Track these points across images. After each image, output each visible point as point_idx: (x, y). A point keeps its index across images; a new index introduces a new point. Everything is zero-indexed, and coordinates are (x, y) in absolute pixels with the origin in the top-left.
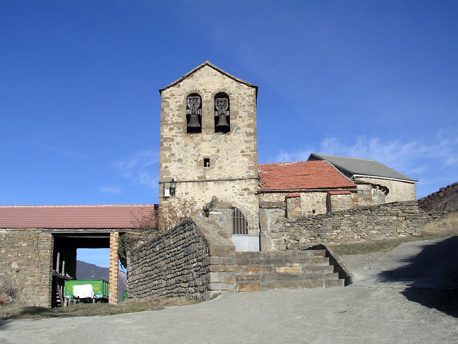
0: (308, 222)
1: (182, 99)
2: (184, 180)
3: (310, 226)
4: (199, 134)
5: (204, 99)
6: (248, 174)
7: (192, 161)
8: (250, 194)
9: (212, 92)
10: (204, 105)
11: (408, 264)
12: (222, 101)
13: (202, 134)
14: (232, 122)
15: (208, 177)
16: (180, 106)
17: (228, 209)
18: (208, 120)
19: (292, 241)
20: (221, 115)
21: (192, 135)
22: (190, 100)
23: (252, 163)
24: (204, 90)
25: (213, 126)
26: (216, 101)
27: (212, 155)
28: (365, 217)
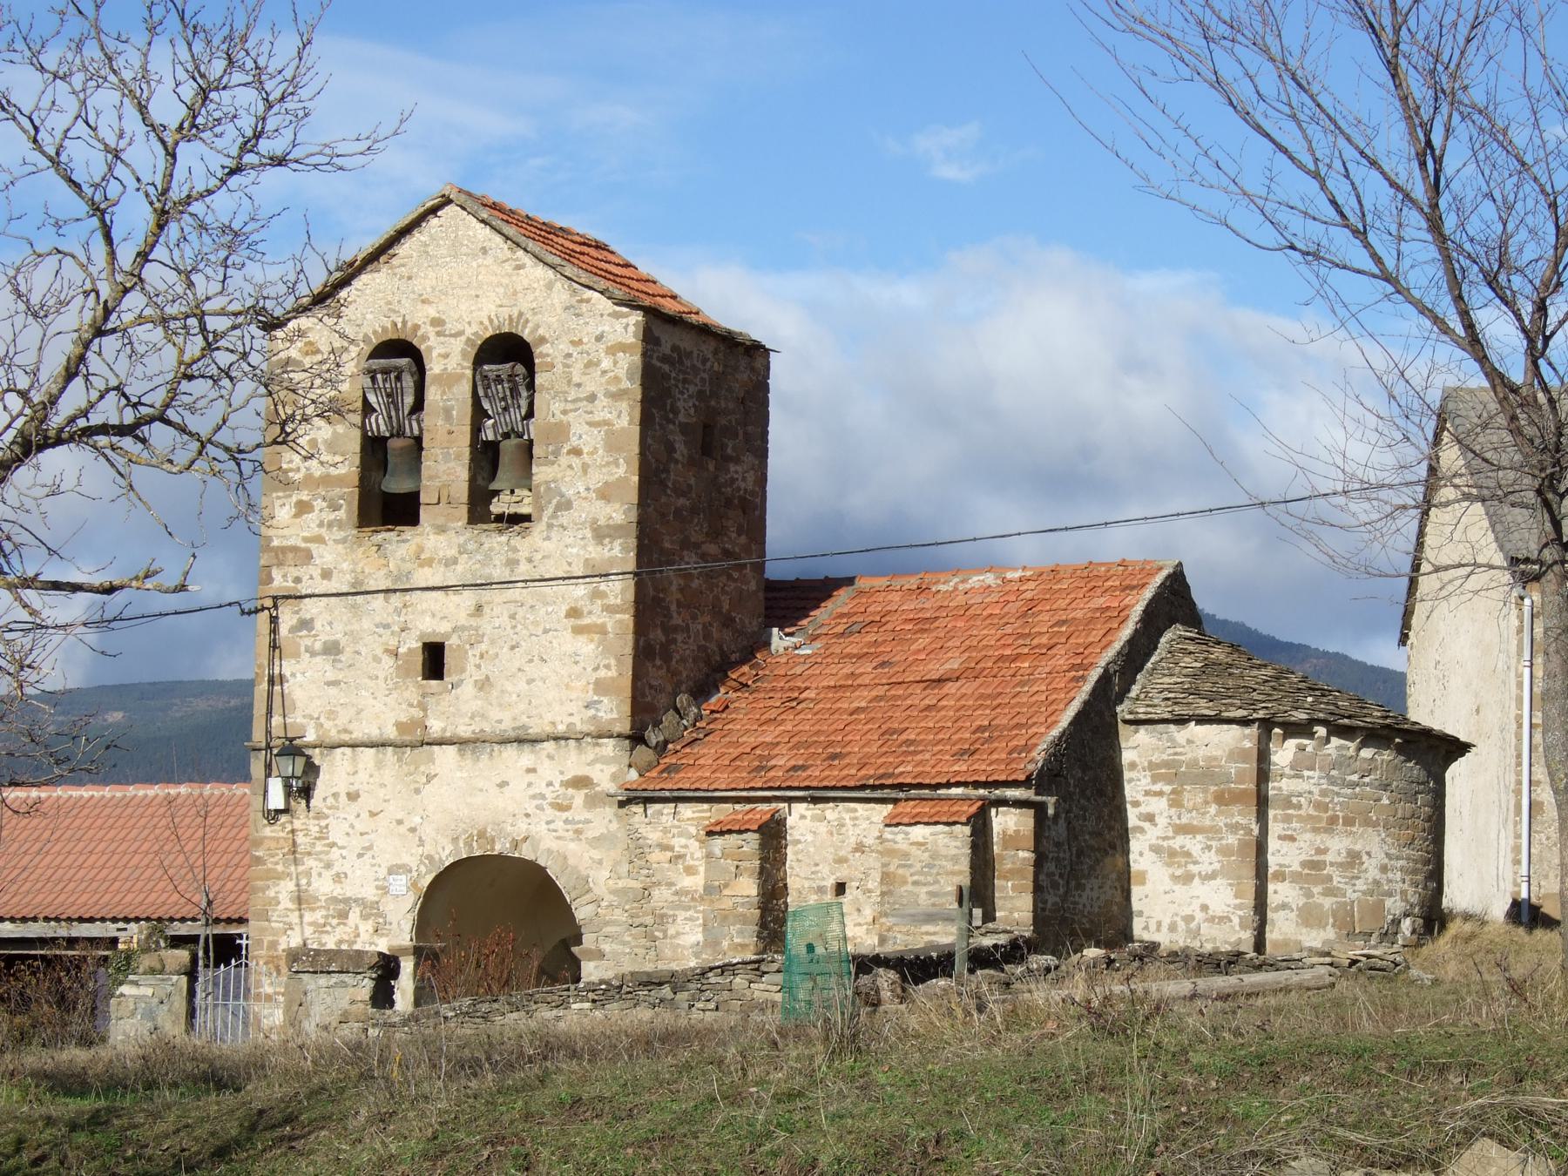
2: (346, 737)
6: (592, 712)
13: (419, 529)
15: (436, 727)
18: (445, 468)
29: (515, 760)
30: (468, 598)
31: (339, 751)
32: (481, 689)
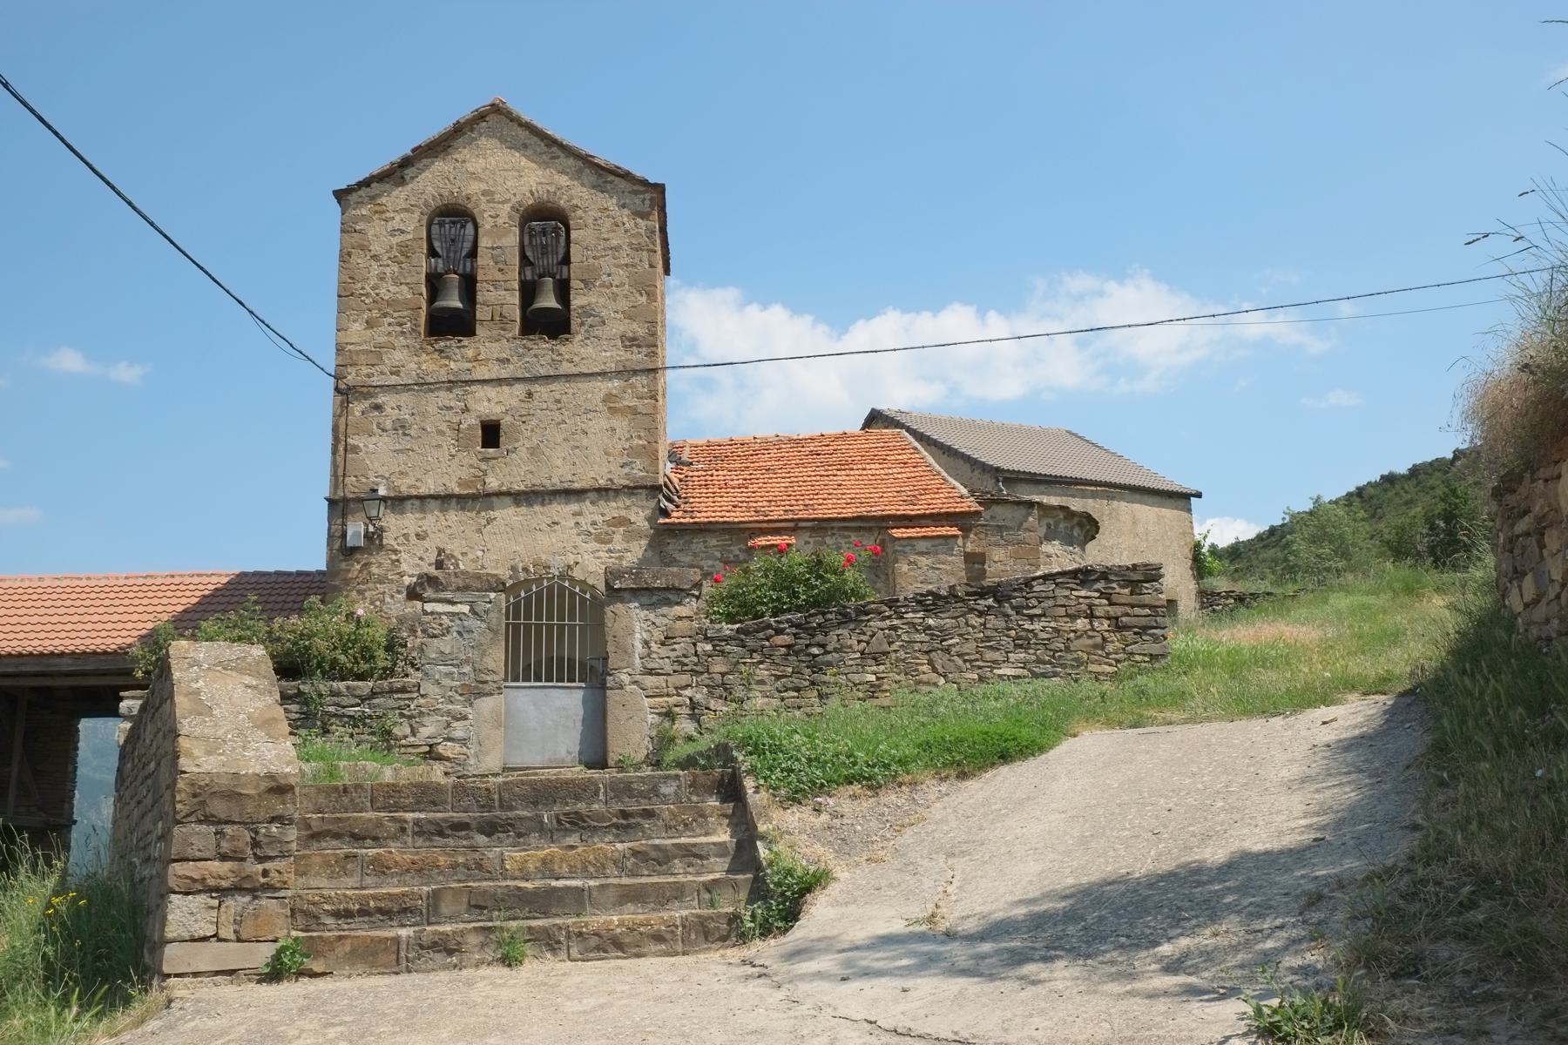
0: (780, 640)
1: (412, 226)
3: (783, 650)
4: (466, 341)
5: (486, 224)
6: (627, 470)
7: (444, 427)
8: (630, 536)
9: (514, 200)
10: (484, 242)
11: (1061, 905)
12: (544, 232)
14: (577, 301)
15: (493, 483)
16: (405, 250)
17: (492, 595)
18: (500, 295)
20: (541, 276)
22: (441, 225)
23: (640, 437)
24: (484, 193)
28: (975, 620)
29: (562, 510)
30: (519, 390)
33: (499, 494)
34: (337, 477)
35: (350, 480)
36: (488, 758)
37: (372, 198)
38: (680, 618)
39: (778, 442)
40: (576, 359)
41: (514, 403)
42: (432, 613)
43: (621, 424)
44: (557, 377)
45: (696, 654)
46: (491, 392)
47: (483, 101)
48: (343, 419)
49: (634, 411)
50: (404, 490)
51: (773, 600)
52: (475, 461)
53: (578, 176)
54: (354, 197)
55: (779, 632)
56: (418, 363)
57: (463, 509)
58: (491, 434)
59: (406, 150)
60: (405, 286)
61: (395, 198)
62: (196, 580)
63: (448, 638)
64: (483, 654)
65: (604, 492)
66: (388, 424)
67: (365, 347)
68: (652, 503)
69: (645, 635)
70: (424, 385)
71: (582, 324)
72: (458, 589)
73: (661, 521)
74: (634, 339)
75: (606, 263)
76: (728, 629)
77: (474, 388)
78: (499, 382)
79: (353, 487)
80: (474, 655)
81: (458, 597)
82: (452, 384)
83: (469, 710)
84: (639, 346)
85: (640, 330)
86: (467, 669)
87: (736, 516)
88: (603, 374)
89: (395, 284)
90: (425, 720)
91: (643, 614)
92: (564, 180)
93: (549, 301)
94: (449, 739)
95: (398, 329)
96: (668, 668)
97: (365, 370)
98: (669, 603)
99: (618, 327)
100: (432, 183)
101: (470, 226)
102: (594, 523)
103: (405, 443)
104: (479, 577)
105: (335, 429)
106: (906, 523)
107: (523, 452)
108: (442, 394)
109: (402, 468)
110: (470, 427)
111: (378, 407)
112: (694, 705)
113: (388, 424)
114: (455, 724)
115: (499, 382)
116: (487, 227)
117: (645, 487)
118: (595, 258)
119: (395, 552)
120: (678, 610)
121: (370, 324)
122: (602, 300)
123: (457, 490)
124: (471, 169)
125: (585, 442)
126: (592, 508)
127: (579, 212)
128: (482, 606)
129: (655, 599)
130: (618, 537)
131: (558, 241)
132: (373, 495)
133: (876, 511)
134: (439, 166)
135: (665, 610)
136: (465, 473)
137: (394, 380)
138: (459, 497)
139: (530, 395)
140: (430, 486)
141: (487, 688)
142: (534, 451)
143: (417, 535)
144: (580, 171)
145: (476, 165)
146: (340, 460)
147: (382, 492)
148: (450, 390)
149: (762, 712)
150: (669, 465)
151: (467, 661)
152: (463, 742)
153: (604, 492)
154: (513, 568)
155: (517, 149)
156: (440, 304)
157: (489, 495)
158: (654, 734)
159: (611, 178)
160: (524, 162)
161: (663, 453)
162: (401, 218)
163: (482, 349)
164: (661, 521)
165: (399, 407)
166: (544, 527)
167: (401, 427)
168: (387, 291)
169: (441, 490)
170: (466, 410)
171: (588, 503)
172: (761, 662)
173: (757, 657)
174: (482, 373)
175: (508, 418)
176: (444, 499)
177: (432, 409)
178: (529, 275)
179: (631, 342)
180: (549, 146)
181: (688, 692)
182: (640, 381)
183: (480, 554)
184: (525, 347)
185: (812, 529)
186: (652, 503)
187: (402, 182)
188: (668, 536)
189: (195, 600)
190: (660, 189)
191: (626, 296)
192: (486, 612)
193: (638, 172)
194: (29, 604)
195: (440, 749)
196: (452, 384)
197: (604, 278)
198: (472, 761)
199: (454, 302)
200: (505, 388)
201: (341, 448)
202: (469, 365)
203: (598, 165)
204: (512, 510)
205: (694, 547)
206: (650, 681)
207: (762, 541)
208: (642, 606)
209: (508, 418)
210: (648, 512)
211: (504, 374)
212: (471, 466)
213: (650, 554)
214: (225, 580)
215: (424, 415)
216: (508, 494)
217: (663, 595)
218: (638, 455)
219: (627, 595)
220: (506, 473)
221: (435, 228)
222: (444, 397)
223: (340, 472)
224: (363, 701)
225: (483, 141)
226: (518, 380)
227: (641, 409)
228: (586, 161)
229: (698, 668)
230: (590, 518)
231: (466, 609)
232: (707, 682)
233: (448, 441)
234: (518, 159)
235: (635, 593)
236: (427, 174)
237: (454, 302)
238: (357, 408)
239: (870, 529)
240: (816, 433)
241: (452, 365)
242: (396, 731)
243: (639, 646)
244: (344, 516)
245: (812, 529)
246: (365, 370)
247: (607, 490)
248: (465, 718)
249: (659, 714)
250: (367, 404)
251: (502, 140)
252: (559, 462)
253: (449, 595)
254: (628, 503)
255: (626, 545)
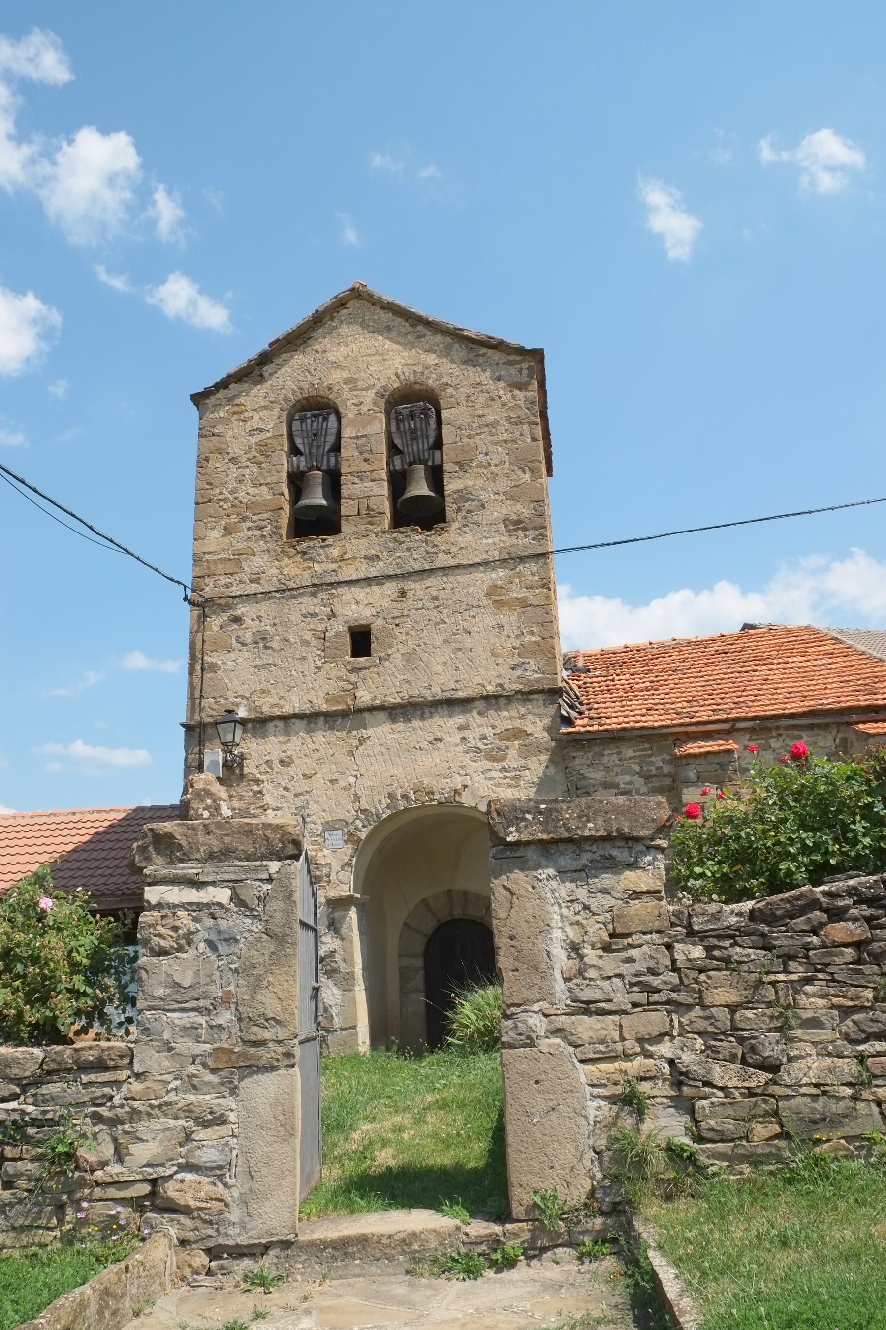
0: (840, 931)
2: (277, 712)
4: (330, 540)
5: (349, 413)
6: (519, 672)
7: (308, 636)
8: (527, 751)
9: (378, 385)
10: (348, 432)
12: (412, 416)
13: (342, 536)
14: (451, 486)
15: (365, 697)
16: (264, 449)
17: (274, 866)
18: (367, 487)
19: (725, 1074)
20: (411, 464)
21: (305, 545)
22: (302, 420)
23: (532, 633)
24: (346, 381)
25: (386, 506)
26: (393, 415)
27: (377, 615)
29: (445, 725)
30: (391, 588)
31: (272, 724)
32: (407, 661)
33: (371, 709)
34: (195, 699)
35: (207, 702)
36: (267, 1207)
37: (230, 399)
38: (637, 895)
39: (678, 646)
40: (454, 549)
41: (386, 603)
42: (159, 906)
43: (510, 619)
44: (432, 571)
45: (674, 968)
46: (359, 593)
47: (342, 287)
48: (200, 635)
49: (524, 604)
50: (267, 711)
51: (805, 850)
52: (343, 673)
53: (446, 352)
54: (211, 401)
55: (837, 915)
56: (280, 568)
57: (331, 728)
58: (361, 641)
59: (264, 346)
60: (266, 487)
61: (254, 396)
62: (95, 816)
63: (191, 953)
64: (256, 986)
65: (493, 700)
66: (248, 638)
67: (223, 555)
68: (552, 710)
69: (572, 933)
70: (286, 591)
71: (459, 510)
72: (211, 856)
73: (564, 730)
74: (520, 522)
75: (482, 441)
76: (734, 913)
77: (340, 590)
78: (368, 581)
79: (211, 709)
80: (236, 987)
81: (209, 871)
82: (316, 588)
83: (230, 1102)
84: (525, 529)
85: (525, 511)
86: (225, 1017)
87: (654, 720)
88: (485, 564)
89: (255, 485)
90: (143, 1127)
91: (564, 889)
92: (431, 359)
93: (421, 488)
94: (189, 1167)
95: (258, 533)
96: (622, 999)
97: (224, 580)
98: (613, 866)
99: (499, 510)
100: (291, 378)
101: (332, 418)
102: (483, 738)
103: (267, 657)
104: (249, 831)
105: (192, 647)
106: (873, 716)
107: (397, 659)
108: (306, 599)
109: (265, 686)
110: (337, 635)
111: (237, 620)
112: (679, 1077)
113: (248, 638)
114: (202, 1134)
115: (368, 581)
116: (351, 416)
117: (541, 691)
118: (469, 437)
119: (257, 782)
120: (633, 879)
121: (228, 531)
122: (480, 482)
123: (324, 707)
124: (332, 358)
125: (468, 642)
126: (480, 720)
127: (450, 390)
128: (253, 889)
129: (585, 858)
130: (512, 753)
131: (428, 424)
132: (229, 717)
133: (829, 703)
134: (299, 359)
135: (606, 879)
136: (333, 688)
137: (254, 588)
138: (327, 715)
139: (403, 593)
140: (295, 704)
141: (265, 1055)
142: (410, 657)
143: (281, 761)
144: (449, 348)
145: (336, 353)
146: (196, 680)
147: (242, 713)
148: (314, 594)
149: (821, 1089)
150: (565, 674)
151: (226, 1001)
152: (217, 1172)
153: (493, 700)
154: (391, 796)
155: (379, 332)
156: (304, 502)
157: (360, 711)
158: (602, 1143)
159: (483, 350)
160: (388, 345)
161: (559, 662)
162: (262, 413)
163: (349, 547)
164: (564, 730)
165: (259, 618)
166: (424, 745)
167: (262, 640)
168: (247, 493)
169: (306, 708)
170: (332, 615)
171: (475, 713)
172: (808, 981)
173: (798, 971)
174: (349, 573)
175: (380, 621)
176: (311, 718)
177: (295, 617)
178: (398, 464)
179: (516, 525)
180: (413, 324)
181: (665, 1049)
182: (528, 569)
183: (352, 780)
184: (395, 540)
185: (752, 730)
186: (552, 710)
187: (261, 379)
188: (574, 748)
189: (87, 838)
190: (538, 355)
191: (507, 476)
192: (262, 899)
193: (513, 339)
194: (66, 832)
195: (171, 1190)
196: (316, 588)
197: (481, 457)
198: (234, 1215)
199: (317, 498)
200: (375, 588)
201: (198, 667)
202: (334, 566)
203: (469, 339)
204: (387, 727)
205: (605, 759)
206: (587, 1027)
207: (693, 748)
208: (562, 873)
209: (380, 621)
210: (547, 721)
211: (373, 572)
212: (340, 679)
213: (552, 771)
214: (123, 815)
215: (286, 624)
216: (382, 708)
217: (599, 850)
218: (532, 654)
219: (531, 854)
220: (381, 683)
221: (296, 425)
222: (308, 603)
223: (197, 695)
224: (24, 1088)
225: (344, 329)
226: (389, 577)
227: (532, 600)
228: (456, 335)
229: (681, 997)
230: (478, 732)
231: (223, 895)
232: (702, 1025)
233: (313, 653)
234: (381, 342)
235: (548, 848)
236: (286, 369)
237: (317, 498)
238: (215, 622)
239: (826, 726)
240: (715, 634)
241: (317, 567)
242: (87, 1153)
243: (560, 954)
244: (201, 743)
245: (752, 730)
246: (224, 580)
247: (496, 697)
248: (222, 1120)
249: (612, 1099)
250: (225, 616)
251: (364, 325)
252: (439, 668)
253: (189, 869)
254: (523, 711)
255: (522, 762)
